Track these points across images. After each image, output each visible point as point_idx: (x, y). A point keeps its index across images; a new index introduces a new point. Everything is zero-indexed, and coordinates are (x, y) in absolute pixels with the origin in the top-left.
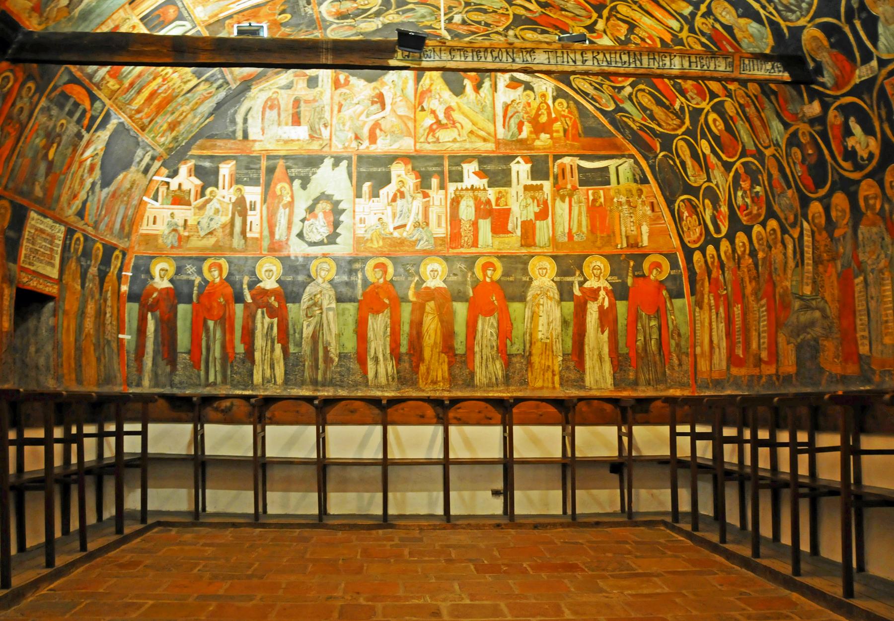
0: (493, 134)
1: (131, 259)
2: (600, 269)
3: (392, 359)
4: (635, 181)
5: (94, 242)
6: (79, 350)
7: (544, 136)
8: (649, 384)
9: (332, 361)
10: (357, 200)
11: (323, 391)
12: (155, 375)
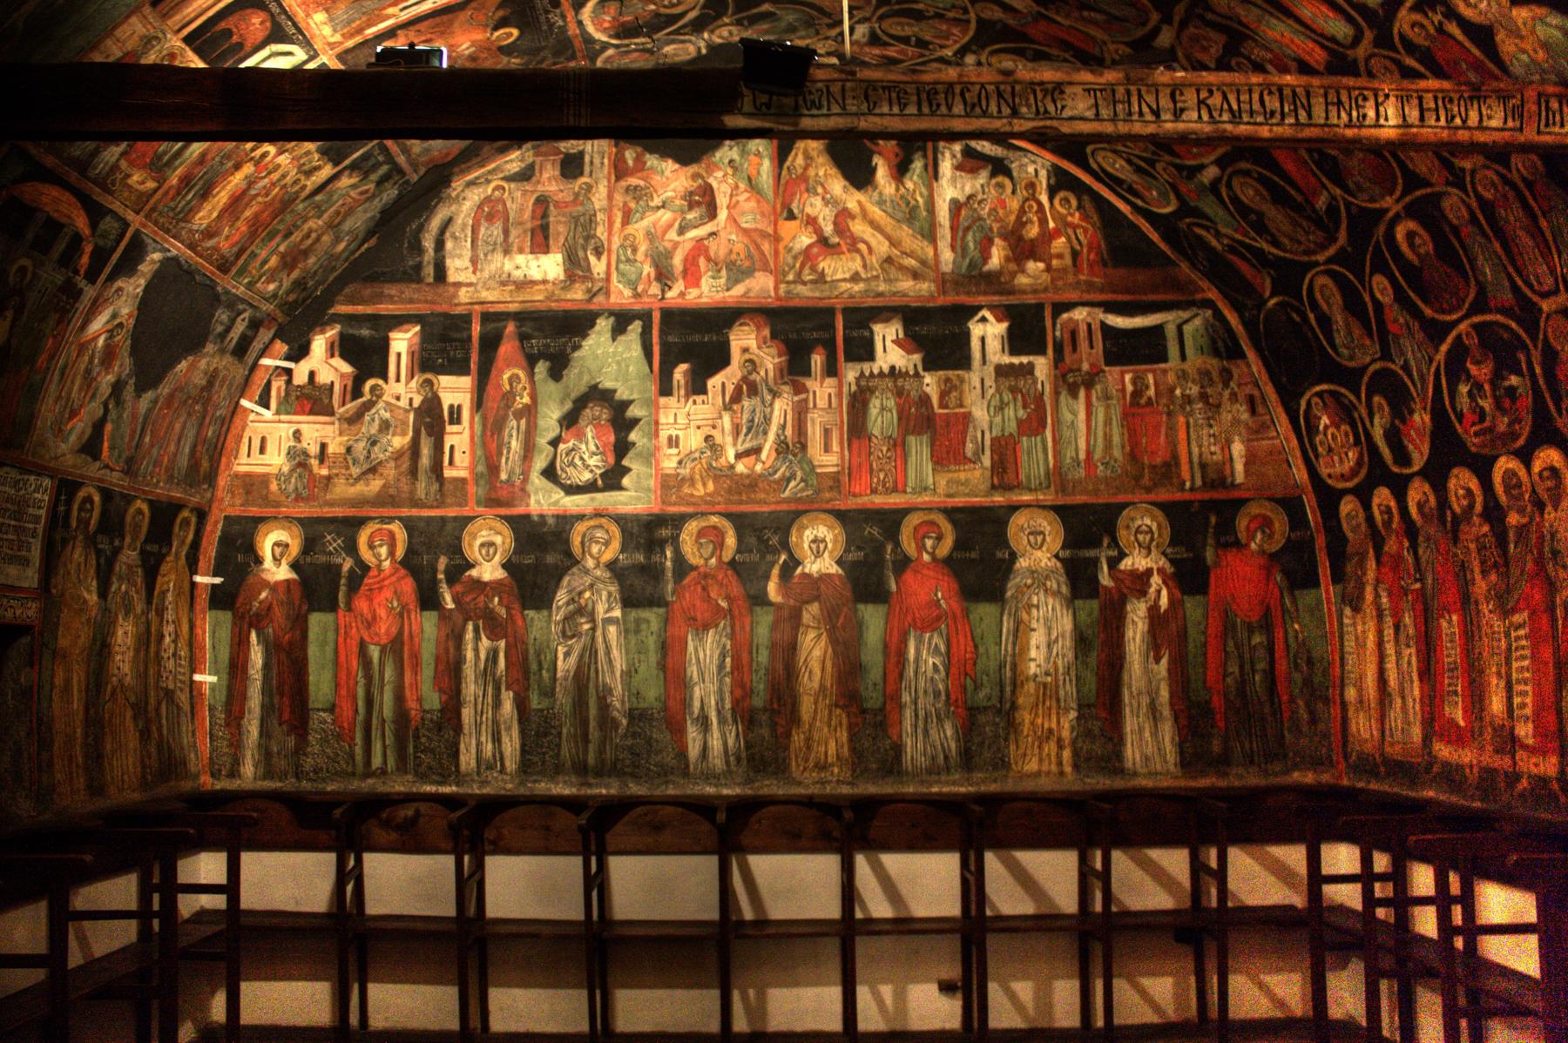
0: (932, 262)
1: (216, 522)
2: (1151, 531)
3: (735, 721)
4: (1216, 353)
5: (129, 500)
6: (95, 724)
7: (1034, 267)
8: (1252, 762)
9: (615, 724)
10: (663, 400)
11: (598, 785)
12: (266, 755)
